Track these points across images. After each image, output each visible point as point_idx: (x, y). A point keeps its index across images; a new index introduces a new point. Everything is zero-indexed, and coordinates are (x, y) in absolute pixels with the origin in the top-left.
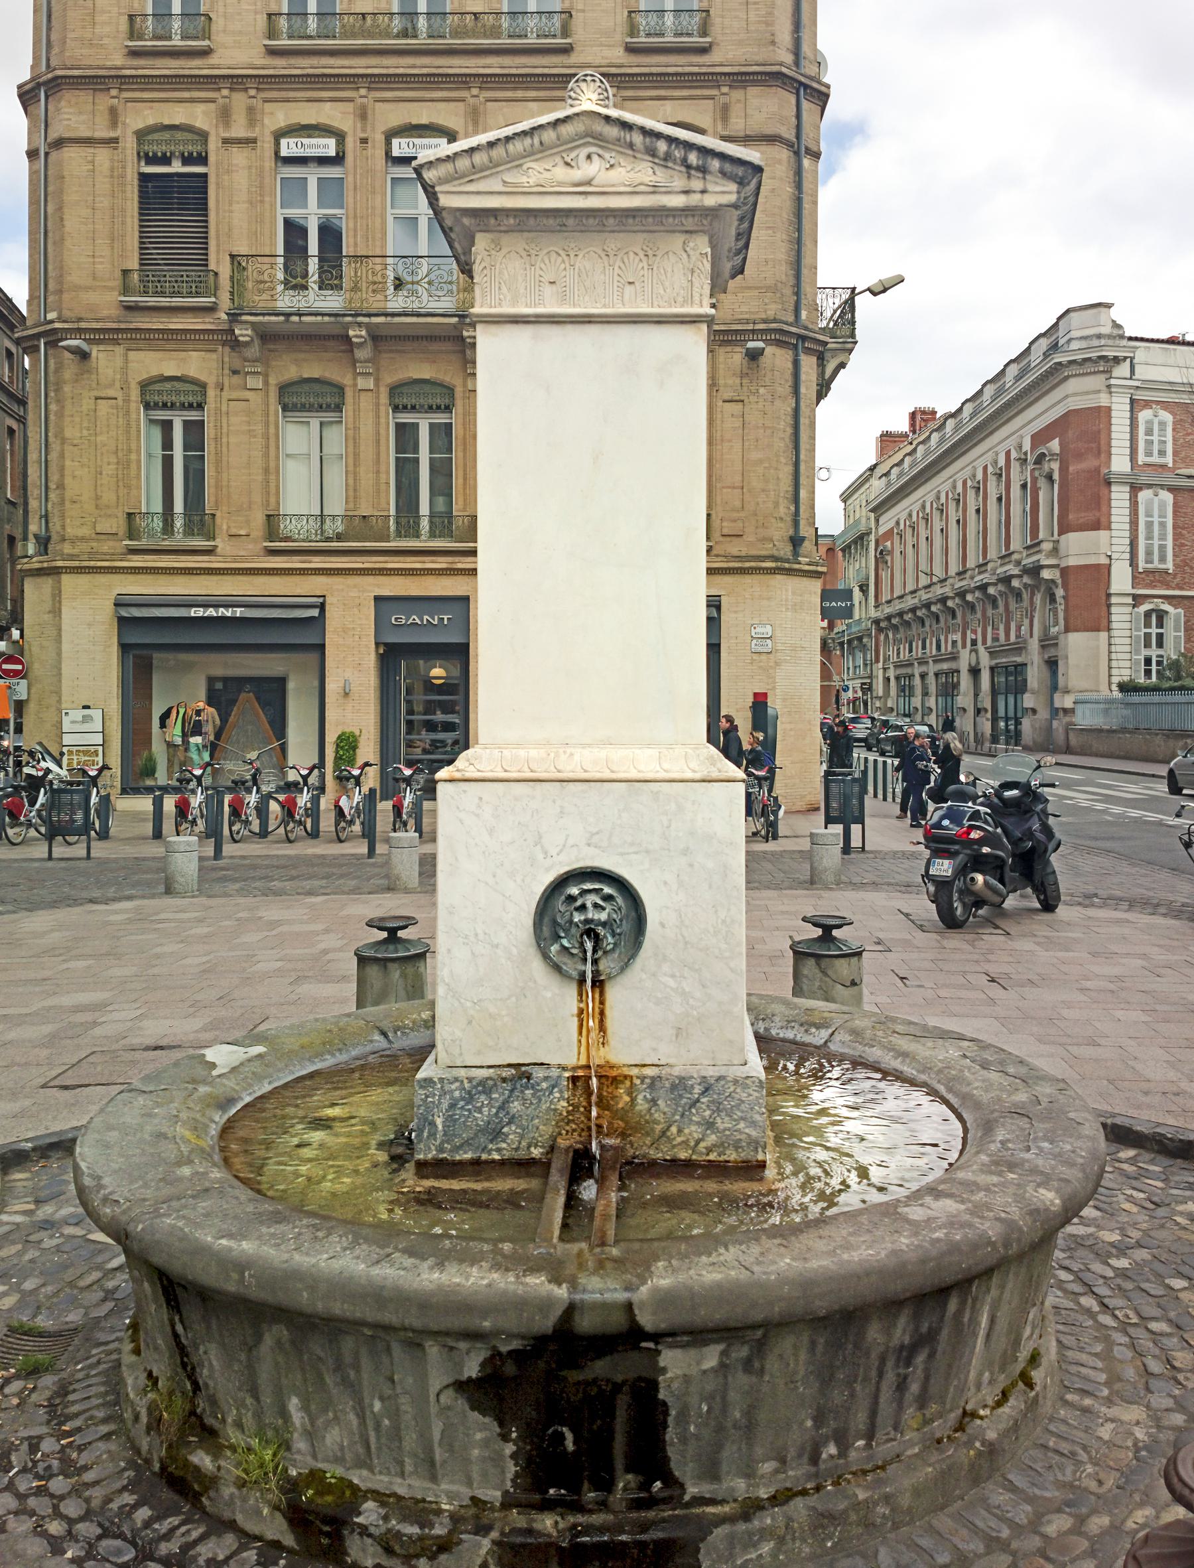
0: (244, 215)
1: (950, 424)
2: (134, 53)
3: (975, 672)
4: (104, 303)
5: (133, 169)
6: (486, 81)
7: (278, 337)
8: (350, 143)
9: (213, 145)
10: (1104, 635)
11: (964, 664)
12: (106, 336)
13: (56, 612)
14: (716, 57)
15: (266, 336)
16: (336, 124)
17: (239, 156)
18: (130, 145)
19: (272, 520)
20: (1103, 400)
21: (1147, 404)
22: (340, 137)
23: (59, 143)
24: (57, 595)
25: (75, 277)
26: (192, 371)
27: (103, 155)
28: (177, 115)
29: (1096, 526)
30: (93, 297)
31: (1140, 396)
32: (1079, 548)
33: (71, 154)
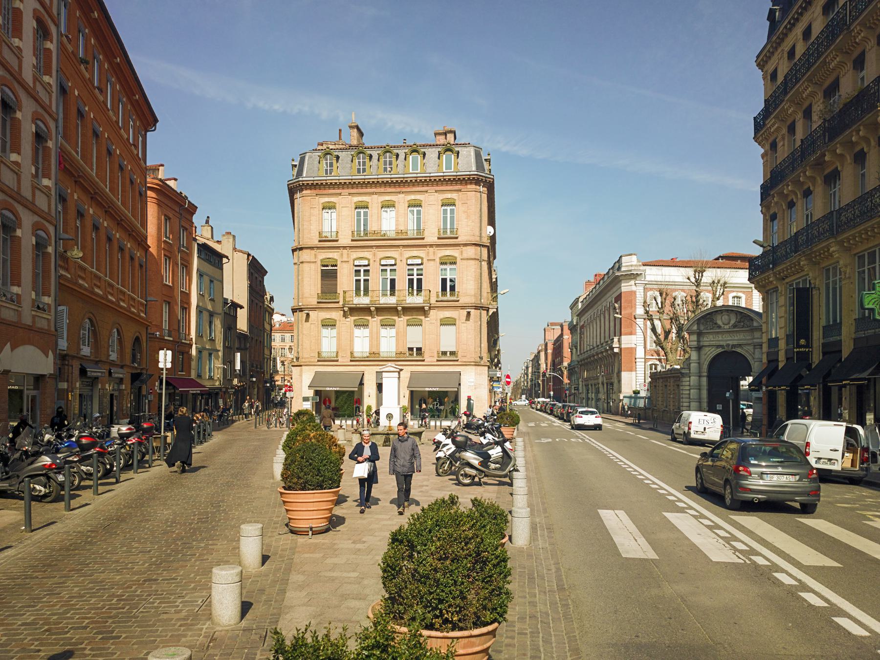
0: (345, 281)
1: (606, 277)
2: (320, 241)
3: (603, 384)
4: (314, 301)
5: (320, 268)
6: (404, 246)
7: (355, 310)
8: (371, 262)
9: (339, 263)
10: (634, 373)
11: (600, 381)
12: (314, 309)
13: (301, 375)
14: (459, 239)
15: (351, 309)
16: (368, 257)
17: (345, 265)
18: (319, 263)
19: (352, 353)
20: (634, 288)
21: (651, 289)
22: (369, 260)
23: (302, 262)
24: (301, 371)
25: (306, 295)
26: (333, 317)
27: (313, 265)
28: (330, 255)
29: (631, 334)
30: (310, 300)
31: (648, 286)
32: (62, 493)
33: (305, 265)
